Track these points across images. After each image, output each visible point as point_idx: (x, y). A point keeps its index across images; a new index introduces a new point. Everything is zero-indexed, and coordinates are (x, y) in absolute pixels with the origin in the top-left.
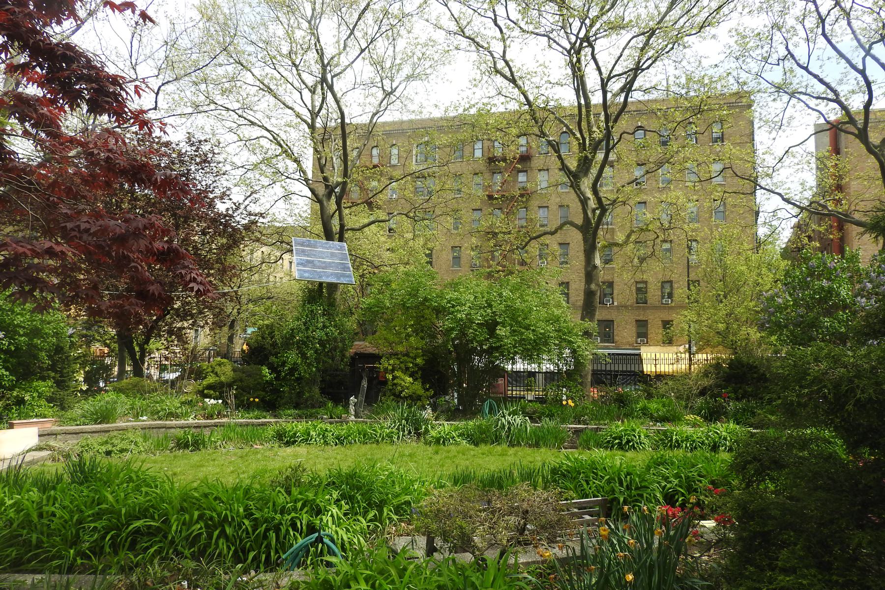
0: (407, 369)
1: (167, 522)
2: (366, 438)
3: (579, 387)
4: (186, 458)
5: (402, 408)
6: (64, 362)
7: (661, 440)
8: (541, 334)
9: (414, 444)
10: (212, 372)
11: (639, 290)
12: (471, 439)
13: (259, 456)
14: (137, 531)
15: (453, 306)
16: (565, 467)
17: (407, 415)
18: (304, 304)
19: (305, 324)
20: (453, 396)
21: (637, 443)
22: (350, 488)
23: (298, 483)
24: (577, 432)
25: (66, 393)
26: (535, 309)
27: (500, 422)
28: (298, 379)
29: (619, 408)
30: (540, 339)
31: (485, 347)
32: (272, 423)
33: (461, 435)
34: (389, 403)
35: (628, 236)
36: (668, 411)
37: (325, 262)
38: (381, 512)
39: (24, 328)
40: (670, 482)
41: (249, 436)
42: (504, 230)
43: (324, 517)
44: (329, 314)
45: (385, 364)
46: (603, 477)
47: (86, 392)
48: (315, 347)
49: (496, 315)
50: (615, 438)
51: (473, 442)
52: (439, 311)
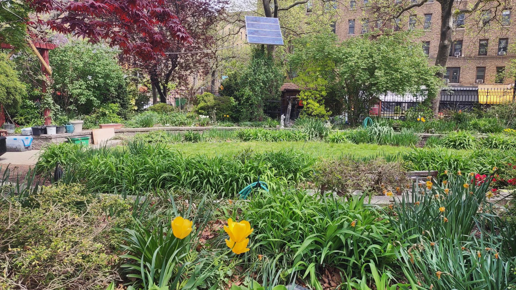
0: (316, 98)
1: (179, 174)
2: (289, 137)
3: (430, 110)
4: (190, 146)
5: (312, 121)
6: (124, 94)
7: (484, 143)
8: (405, 74)
9: (319, 142)
10: (203, 100)
11: (481, 46)
12: (354, 140)
13: (229, 146)
14: (165, 179)
15: (347, 58)
16: (413, 156)
17: (315, 125)
18: (253, 59)
19: (254, 71)
20: (345, 115)
21: (467, 145)
22: (278, 162)
23: (249, 158)
24: (425, 138)
25: (126, 111)
26: (402, 58)
27: (373, 130)
28: (251, 104)
29: (457, 124)
30: (405, 78)
31: (367, 84)
32: (237, 128)
33: (347, 138)
34: (304, 119)
35: (477, 5)
36: (492, 126)
37: (265, 31)
38: (295, 175)
39: (101, 74)
40: (486, 167)
41: (224, 136)
42: (385, 5)
43: (263, 176)
44: (268, 65)
45: (302, 95)
46: (438, 162)
47: (137, 111)
48: (260, 85)
49: (375, 63)
50: (451, 142)
51: (356, 142)
52: (337, 61)
